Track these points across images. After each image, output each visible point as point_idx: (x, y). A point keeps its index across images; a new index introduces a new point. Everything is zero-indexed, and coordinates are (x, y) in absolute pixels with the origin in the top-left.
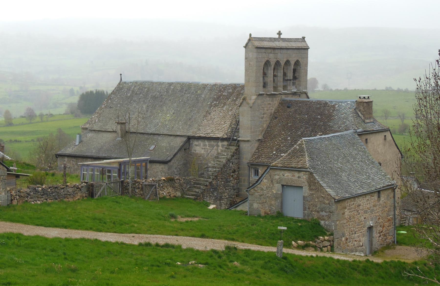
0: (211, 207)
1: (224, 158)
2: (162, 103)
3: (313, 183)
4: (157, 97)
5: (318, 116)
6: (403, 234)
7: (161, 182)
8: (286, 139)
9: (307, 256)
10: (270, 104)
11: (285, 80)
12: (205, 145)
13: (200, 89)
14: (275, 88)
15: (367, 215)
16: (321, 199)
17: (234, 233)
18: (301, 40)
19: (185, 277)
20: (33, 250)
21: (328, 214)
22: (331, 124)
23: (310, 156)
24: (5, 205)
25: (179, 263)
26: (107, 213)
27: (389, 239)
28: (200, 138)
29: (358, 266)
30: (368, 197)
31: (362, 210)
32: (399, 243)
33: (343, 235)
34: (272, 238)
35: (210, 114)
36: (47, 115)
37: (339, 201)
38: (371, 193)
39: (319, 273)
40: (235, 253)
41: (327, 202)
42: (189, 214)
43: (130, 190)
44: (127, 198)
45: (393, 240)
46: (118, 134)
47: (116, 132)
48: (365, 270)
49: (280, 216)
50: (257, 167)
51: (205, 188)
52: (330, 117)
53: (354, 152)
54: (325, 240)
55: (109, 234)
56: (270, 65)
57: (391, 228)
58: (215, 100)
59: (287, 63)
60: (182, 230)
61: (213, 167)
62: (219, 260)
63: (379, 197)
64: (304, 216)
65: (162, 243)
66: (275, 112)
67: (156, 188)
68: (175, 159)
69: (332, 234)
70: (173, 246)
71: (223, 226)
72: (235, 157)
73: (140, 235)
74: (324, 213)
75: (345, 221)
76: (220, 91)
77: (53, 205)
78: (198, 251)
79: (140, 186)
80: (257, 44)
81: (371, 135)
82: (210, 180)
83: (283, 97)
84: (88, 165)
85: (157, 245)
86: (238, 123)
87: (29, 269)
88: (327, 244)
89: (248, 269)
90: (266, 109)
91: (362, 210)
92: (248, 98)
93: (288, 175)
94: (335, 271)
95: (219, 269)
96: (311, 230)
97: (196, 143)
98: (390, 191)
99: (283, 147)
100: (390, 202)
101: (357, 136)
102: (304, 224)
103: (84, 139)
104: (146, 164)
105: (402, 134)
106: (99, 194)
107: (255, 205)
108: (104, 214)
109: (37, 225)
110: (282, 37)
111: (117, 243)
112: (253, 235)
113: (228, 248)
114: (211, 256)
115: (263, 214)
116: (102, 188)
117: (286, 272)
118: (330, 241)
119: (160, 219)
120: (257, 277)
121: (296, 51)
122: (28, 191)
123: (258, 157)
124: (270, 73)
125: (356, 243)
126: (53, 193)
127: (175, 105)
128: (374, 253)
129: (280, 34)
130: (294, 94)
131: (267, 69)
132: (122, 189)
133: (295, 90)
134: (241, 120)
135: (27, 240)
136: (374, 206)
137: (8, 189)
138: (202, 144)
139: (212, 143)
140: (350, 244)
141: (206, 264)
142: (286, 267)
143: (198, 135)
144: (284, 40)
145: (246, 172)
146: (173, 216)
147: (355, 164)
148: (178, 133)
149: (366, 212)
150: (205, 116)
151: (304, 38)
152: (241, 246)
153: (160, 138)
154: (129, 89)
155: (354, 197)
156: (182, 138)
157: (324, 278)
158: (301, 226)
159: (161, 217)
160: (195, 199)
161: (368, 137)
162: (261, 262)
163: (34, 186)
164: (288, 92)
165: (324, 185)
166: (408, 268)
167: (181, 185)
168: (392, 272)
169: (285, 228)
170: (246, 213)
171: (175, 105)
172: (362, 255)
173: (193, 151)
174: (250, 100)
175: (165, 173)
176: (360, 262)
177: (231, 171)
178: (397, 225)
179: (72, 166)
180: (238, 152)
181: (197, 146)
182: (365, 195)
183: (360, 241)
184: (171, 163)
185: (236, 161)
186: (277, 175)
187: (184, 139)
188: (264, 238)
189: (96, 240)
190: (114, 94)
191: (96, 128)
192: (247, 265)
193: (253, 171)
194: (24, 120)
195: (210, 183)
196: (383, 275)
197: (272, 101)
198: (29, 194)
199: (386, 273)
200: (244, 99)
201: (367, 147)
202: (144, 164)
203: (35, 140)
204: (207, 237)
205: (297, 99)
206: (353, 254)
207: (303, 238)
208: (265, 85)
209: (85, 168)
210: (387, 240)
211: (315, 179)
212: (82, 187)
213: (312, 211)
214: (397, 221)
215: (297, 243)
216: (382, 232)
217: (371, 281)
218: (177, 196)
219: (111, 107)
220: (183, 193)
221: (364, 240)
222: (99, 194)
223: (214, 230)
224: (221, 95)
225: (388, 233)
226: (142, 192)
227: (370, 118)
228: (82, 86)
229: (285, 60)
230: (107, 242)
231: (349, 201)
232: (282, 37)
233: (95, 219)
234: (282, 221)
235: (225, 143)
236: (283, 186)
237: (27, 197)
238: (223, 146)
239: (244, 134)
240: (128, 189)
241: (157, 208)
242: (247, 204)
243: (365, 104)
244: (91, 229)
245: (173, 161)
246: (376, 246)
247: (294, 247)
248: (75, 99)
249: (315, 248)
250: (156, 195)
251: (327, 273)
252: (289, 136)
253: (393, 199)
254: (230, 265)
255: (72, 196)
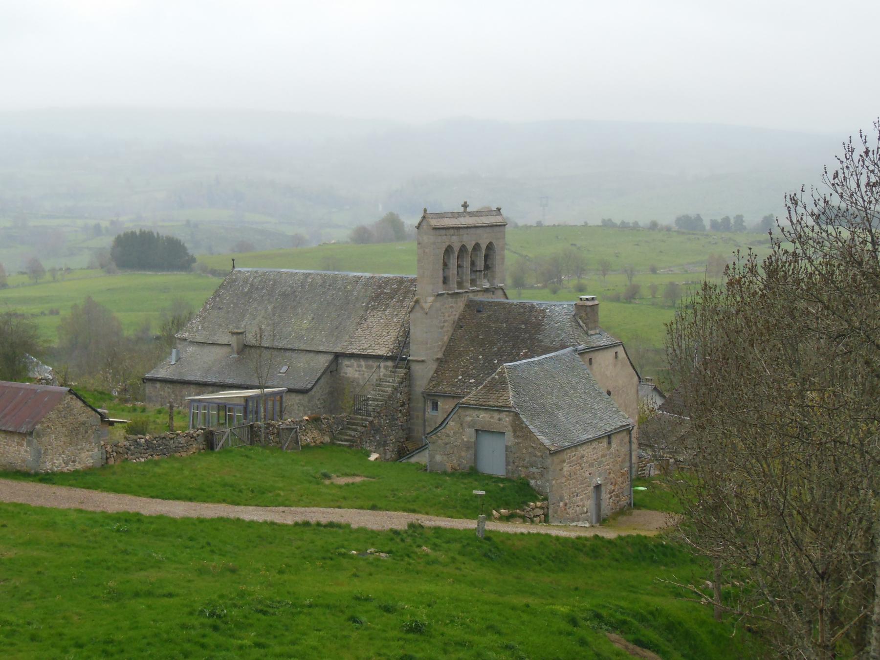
0: (373, 457)
1: (389, 386)
2: (295, 303)
3: (519, 428)
4: (288, 295)
5: (522, 332)
6: (641, 491)
7: (303, 424)
8: (477, 360)
9: (516, 534)
10: (452, 307)
11: (474, 271)
12: (360, 366)
13: (350, 283)
14: (460, 285)
15: (591, 470)
16: (530, 450)
17: (414, 501)
18: (494, 213)
19: (371, 574)
20: (165, 539)
21: (539, 471)
22: (540, 337)
23: (515, 389)
24: (99, 466)
25: (354, 552)
26: (238, 475)
27: (624, 501)
28: (352, 356)
29: (584, 546)
30: (594, 444)
31: (586, 462)
32: (637, 506)
33: (561, 499)
34: (469, 508)
35: (365, 320)
36: (61, 269)
37: (556, 453)
38: (598, 439)
39: (534, 558)
40: (421, 534)
41: (539, 454)
42: (348, 471)
43: (263, 436)
44: (260, 449)
45: (628, 501)
46: (232, 348)
47: (229, 345)
48: (593, 551)
49: (473, 473)
50: (436, 398)
51: (364, 429)
52: (538, 327)
53: (574, 381)
54: (537, 507)
55: (251, 508)
56: (453, 252)
57: (626, 485)
58: (372, 299)
59: (477, 247)
60: (345, 498)
61: (374, 400)
62: (402, 545)
63: (609, 443)
64: (507, 473)
65: (324, 521)
66: (459, 319)
67: (296, 432)
68: (317, 386)
69: (546, 499)
70: (339, 526)
71: (397, 490)
72: (404, 384)
73: (292, 509)
74: (534, 470)
75: (563, 480)
76: (380, 287)
77: (163, 465)
78: (372, 531)
79: (276, 431)
80: (435, 223)
81: (596, 353)
82: (371, 419)
83: (471, 296)
84: (199, 401)
85: (319, 524)
86: (407, 334)
87: (175, 569)
88: (539, 512)
89: (442, 557)
90: (447, 314)
91: (586, 462)
92: (422, 301)
93: (483, 416)
94: (554, 555)
95: (406, 559)
96: (519, 493)
97: (346, 362)
98: (625, 433)
99: (472, 370)
100: (624, 450)
101: (577, 356)
102: (508, 484)
103: (183, 355)
104: (281, 397)
105: (630, 302)
106: (221, 444)
107: (438, 458)
108: (235, 476)
109: (152, 497)
110: (468, 210)
111: (265, 522)
112: (440, 503)
113: (411, 526)
114: (392, 539)
115: (449, 470)
116: (224, 438)
117: (492, 559)
118: (543, 508)
119: (310, 482)
120: (457, 568)
121: (488, 230)
122: (127, 444)
123: (438, 384)
124: (453, 262)
125: (578, 509)
126: (160, 445)
127: (315, 306)
128: (602, 521)
129: (465, 206)
130: (486, 290)
131: (449, 258)
132: (252, 436)
133: (487, 285)
134: (412, 331)
135: (152, 523)
136: (604, 456)
137: (102, 443)
138: (355, 364)
139: (370, 362)
140: (570, 511)
141: (389, 552)
142: (490, 551)
143: (350, 351)
144: (471, 214)
145: (420, 405)
146: (326, 476)
147: (576, 397)
148: (321, 349)
149: (591, 465)
150: (359, 324)
151: (499, 209)
152: (430, 521)
153: (294, 355)
154: (246, 281)
155: (576, 446)
156: (325, 355)
157: (540, 565)
158: (503, 489)
159: (311, 479)
160: (350, 447)
161: (592, 355)
162: (458, 546)
163: (134, 437)
164: (478, 289)
165: (535, 430)
166: (651, 546)
167: (330, 427)
168: (630, 550)
169: (484, 493)
170: (425, 469)
171: (315, 306)
172: (587, 525)
173: (342, 374)
174: (426, 302)
175: (305, 407)
176: (586, 539)
177: (399, 404)
178: (633, 477)
179: (166, 394)
180: (408, 378)
181: (348, 366)
182: (590, 441)
183: (583, 506)
184: (312, 393)
185: (406, 390)
186: (470, 417)
187: (330, 357)
188: (455, 507)
189: (238, 519)
190: (223, 289)
191: (199, 338)
192: (440, 550)
193: (429, 404)
194: (25, 278)
195: (371, 422)
196: (618, 556)
197: (456, 302)
198: (129, 449)
199: (622, 553)
200: (417, 302)
201: (591, 369)
202: (278, 398)
203: (47, 312)
204: (380, 509)
205: (490, 300)
206: (574, 524)
207: (507, 505)
208: (445, 281)
209: (196, 404)
210: (621, 503)
211: (522, 422)
212: (198, 435)
213: (517, 467)
214: (634, 473)
215: (500, 513)
216: (614, 491)
217: (602, 566)
218: (325, 441)
219: (220, 308)
220: (333, 438)
221: (590, 504)
222: (221, 444)
223: (386, 497)
224: (382, 293)
225: (622, 493)
226: (277, 439)
227: (595, 328)
228: (115, 219)
229: (474, 243)
230: (252, 521)
231: (569, 451)
232: (468, 210)
233: (225, 485)
234: (476, 480)
235: (390, 363)
236: (477, 431)
237: (127, 453)
238: (386, 367)
239: (416, 352)
240: (259, 436)
241: (303, 463)
242: (426, 453)
243: (588, 309)
244: (224, 501)
245: (314, 389)
246: (606, 511)
247: (496, 518)
248: (107, 241)
249: (524, 519)
250: (297, 443)
251: (543, 558)
252: (481, 354)
253: (628, 444)
254: (417, 550)
255: (185, 449)
